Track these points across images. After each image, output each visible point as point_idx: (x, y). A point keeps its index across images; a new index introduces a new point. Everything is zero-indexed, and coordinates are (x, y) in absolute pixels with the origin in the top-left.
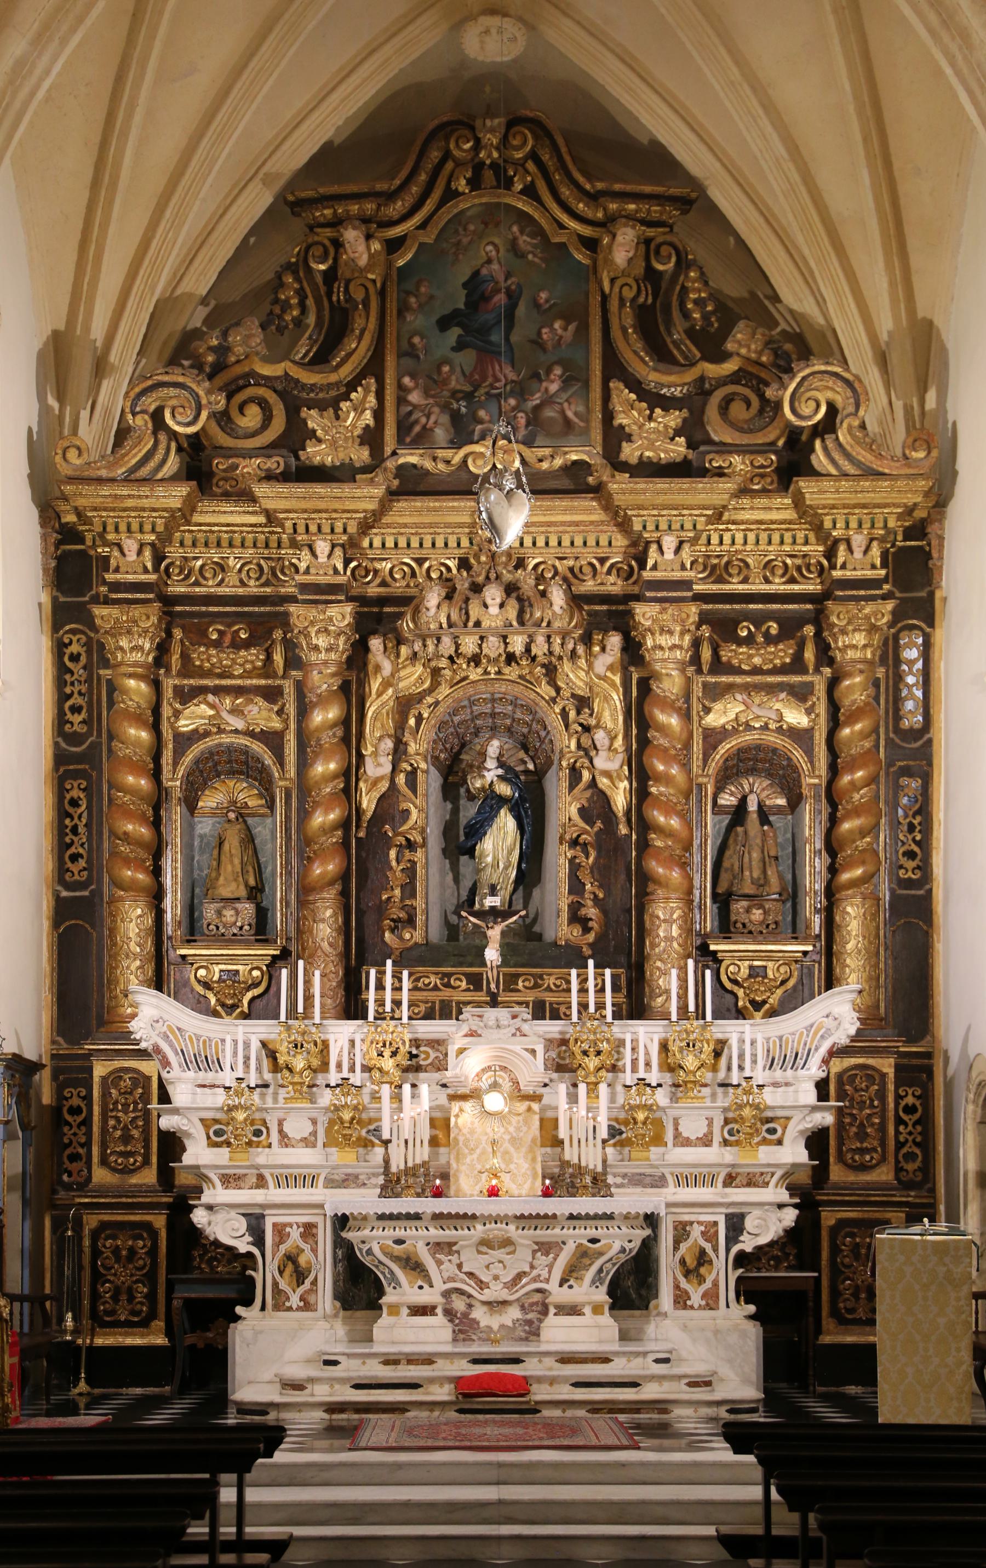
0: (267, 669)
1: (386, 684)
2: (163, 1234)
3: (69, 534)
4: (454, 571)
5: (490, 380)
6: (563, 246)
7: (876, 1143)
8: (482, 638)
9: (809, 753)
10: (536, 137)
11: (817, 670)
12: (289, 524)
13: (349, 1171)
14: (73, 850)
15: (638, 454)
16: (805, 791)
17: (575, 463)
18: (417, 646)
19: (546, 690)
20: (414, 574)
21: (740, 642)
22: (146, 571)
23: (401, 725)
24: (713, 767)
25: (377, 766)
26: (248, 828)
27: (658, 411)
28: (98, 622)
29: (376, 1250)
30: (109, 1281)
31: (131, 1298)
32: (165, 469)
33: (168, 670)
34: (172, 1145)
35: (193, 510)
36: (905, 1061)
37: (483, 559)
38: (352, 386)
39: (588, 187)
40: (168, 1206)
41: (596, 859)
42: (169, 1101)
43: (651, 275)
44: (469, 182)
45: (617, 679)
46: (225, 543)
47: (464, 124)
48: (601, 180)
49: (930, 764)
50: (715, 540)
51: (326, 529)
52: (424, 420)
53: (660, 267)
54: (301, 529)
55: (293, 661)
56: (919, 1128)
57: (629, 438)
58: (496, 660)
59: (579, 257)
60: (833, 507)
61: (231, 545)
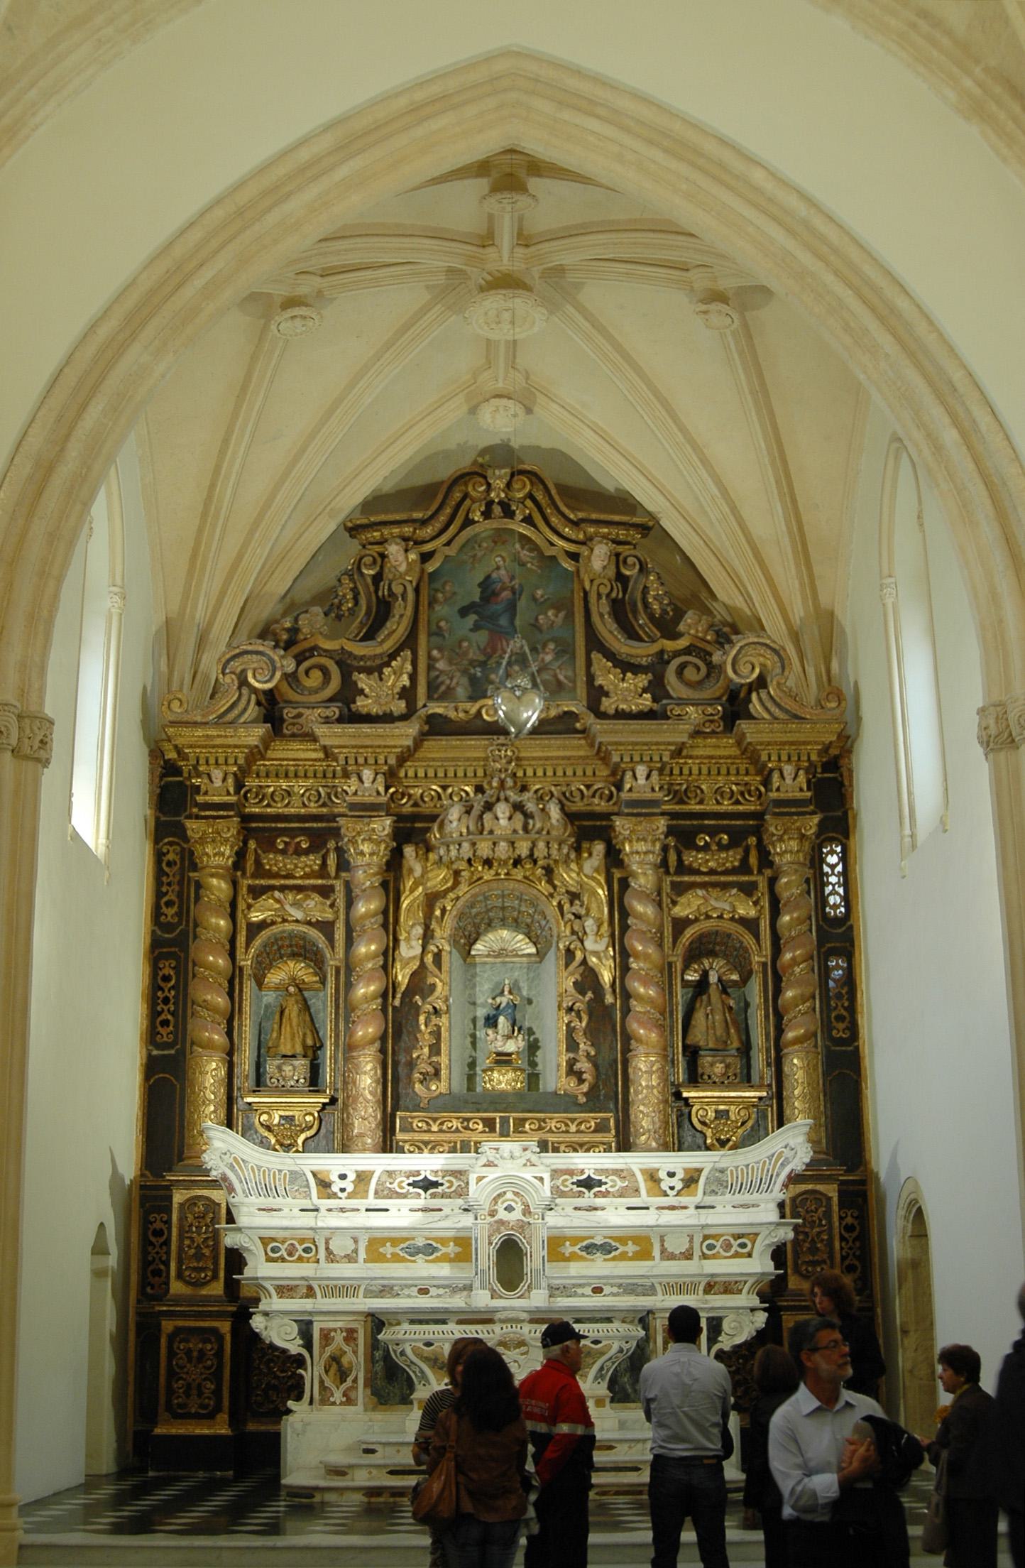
0: (323, 872)
1: (416, 884)
2: (228, 1338)
3: (170, 769)
4: (472, 795)
5: (499, 652)
6: (553, 558)
7: (825, 1256)
8: (494, 844)
9: (757, 937)
10: (532, 483)
11: (760, 872)
12: (342, 757)
13: (385, 1282)
14: (163, 1017)
15: (613, 707)
16: (755, 967)
17: (565, 713)
18: (442, 852)
19: (544, 886)
20: (440, 798)
21: (699, 849)
22: (228, 794)
23: (429, 915)
24: (680, 950)
25: (410, 949)
26: (305, 1000)
27: (629, 675)
28: (189, 833)
29: (409, 1351)
30: (181, 1378)
31: (200, 1394)
32: (246, 715)
33: (244, 874)
34: (236, 1260)
35: (267, 748)
36: (844, 1188)
37: (495, 784)
38: (393, 656)
39: (572, 516)
40: (233, 1314)
41: (588, 1024)
42: (234, 1222)
43: (621, 578)
44: (483, 513)
45: (602, 879)
46: (291, 774)
47: (477, 473)
48: (580, 510)
49: (853, 945)
50: (676, 771)
51: (371, 761)
52: (448, 682)
53: (628, 573)
54: (351, 761)
55: (343, 865)
56: (858, 1244)
57: (607, 695)
58: (505, 862)
59: (565, 565)
60: (769, 744)
61: (296, 776)
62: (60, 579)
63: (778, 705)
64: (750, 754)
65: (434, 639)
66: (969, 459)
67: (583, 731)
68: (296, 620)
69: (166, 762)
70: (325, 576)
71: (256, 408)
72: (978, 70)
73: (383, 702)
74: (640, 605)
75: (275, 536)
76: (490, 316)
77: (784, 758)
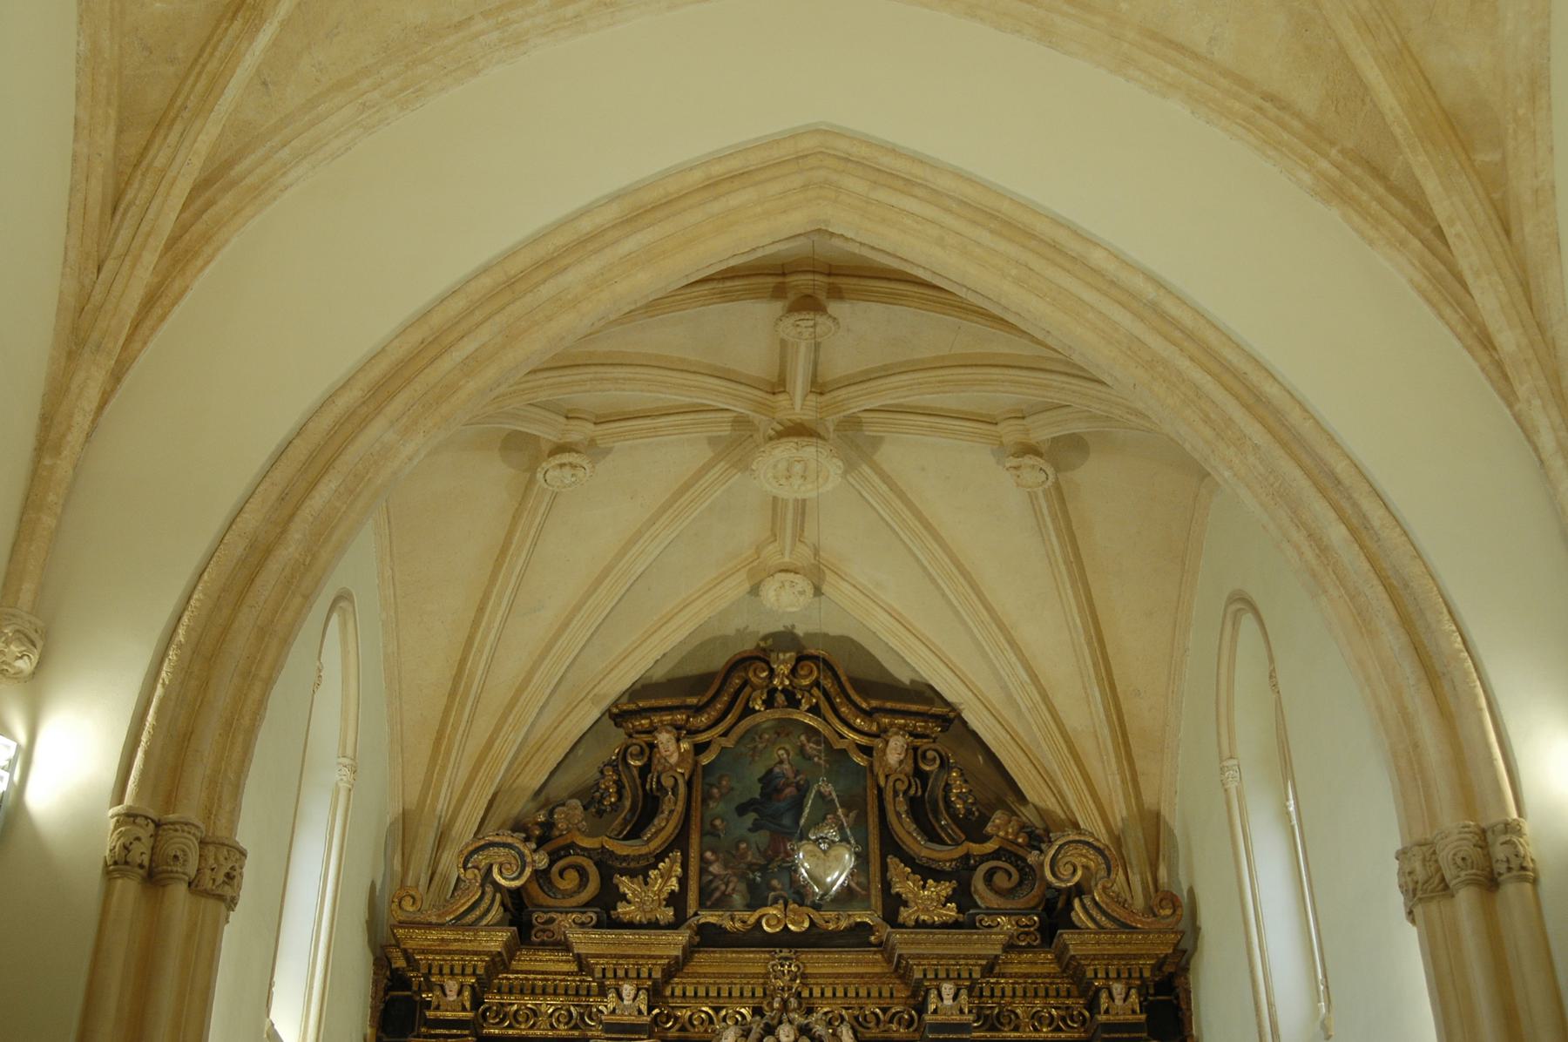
4: (749, 1018)
6: (844, 752)
17: (858, 924)
20: (711, 1021)
22: (464, 1009)
27: (930, 881)
32: (489, 917)
35: (511, 958)
37: (776, 1005)
38: (660, 857)
39: (864, 705)
43: (919, 773)
46: (538, 991)
47: (759, 657)
48: (876, 698)
50: (987, 993)
51: (633, 974)
52: (723, 887)
53: (927, 768)
54: (609, 974)
59: (857, 759)
60: (1095, 957)
61: (544, 993)
62: (269, 683)
63: (1104, 913)
64: (1071, 969)
65: (707, 839)
66: (1363, 558)
67: (880, 944)
68: (551, 813)
69: (394, 972)
70: (585, 771)
71: (516, 572)
72: (1334, 152)
73: (647, 908)
74: (941, 804)
75: (530, 720)
76: (782, 470)
77: (1113, 975)
